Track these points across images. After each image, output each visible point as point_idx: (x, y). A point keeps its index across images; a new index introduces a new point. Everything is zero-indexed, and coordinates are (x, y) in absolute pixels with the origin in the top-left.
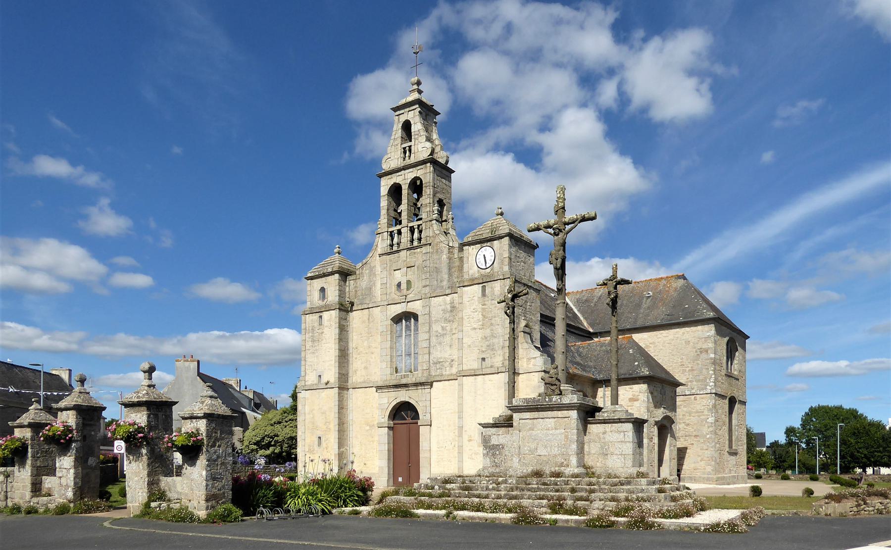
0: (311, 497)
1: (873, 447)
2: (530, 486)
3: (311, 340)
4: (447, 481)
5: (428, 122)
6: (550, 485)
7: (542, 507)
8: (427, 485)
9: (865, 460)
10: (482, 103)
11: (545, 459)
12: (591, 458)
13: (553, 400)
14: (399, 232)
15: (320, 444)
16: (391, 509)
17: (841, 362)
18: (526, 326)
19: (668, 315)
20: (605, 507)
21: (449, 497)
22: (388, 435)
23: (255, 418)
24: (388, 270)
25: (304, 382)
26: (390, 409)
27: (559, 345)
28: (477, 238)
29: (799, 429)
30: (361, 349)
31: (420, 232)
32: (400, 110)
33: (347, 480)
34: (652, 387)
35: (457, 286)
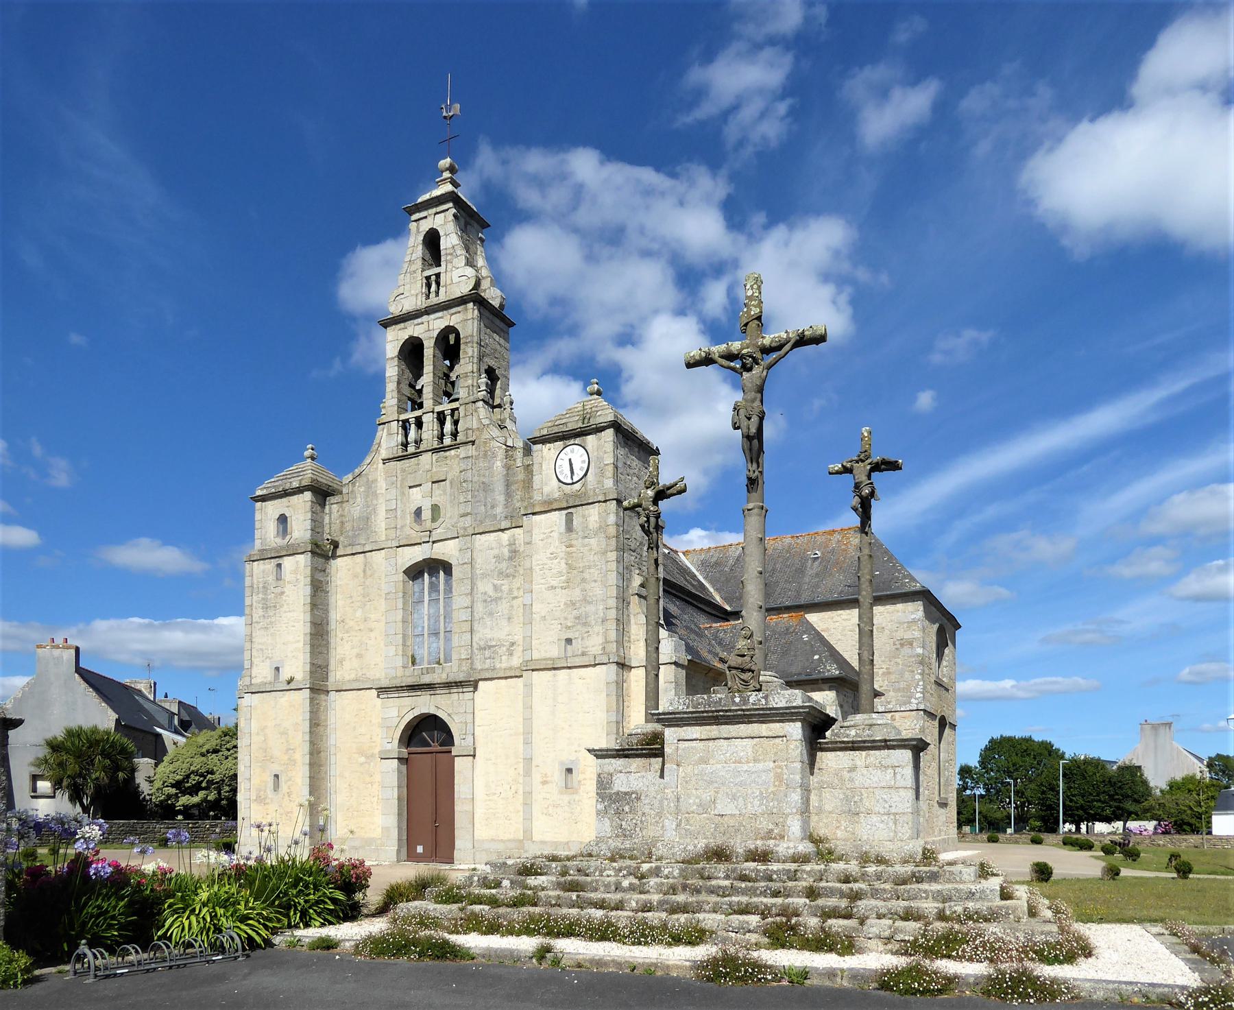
0: (222, 911)
1: (1091, 794)
2: (714, 882)
3: (261, 605)
4: (528, 870)
5: (469, 237)
6: (755, 880)
7: (749, 931)
8: (485, 878)
9: (1081, 812)
10: (537, 298)
11: (732, 822)
13: (751, 701)
14: (419, 423)
15: (276, 787)
16: (407, 940)
17: (1007, 681)
18: (642, 585)
19: (849, 586)
21: (535, 905)
22: (399, 771)
23: (175, 743)
24: (399, 486)
25: (248, 679)
26: (402, 727)
27: (753, 593)
28: (556, 430)
29: (976, 768)
30: (351, 623)
31: (456, 423)
32: (419, 212)
33: (311, 868)
34: (842, 697)
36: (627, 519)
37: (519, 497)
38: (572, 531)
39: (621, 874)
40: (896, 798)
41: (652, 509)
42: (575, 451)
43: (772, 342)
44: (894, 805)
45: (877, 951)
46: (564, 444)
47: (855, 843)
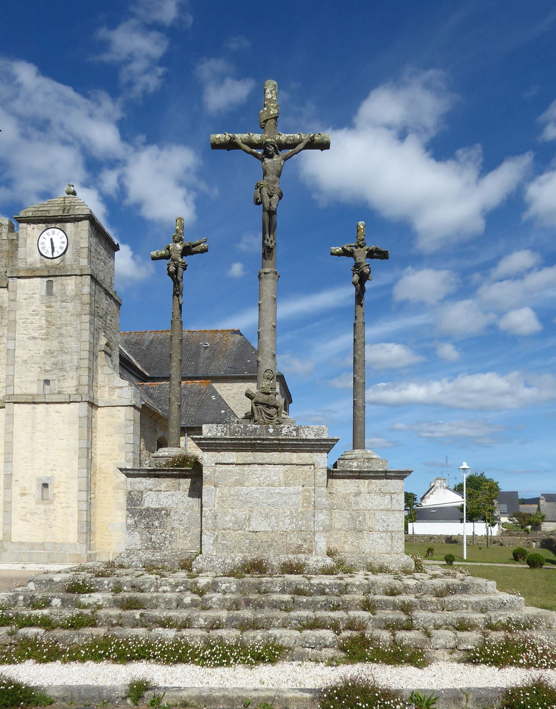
7: (326, 646)
11: (265, 538)
12: (335, 536)
13: (284, 432)
18: (107, 345)
20: (459, 643)
21: (94, 625)
27: (268, 343)
28: (39, 214)
35: (8, 274)
36: (97, 292)
37: (4, 264)
38: (51, 295)
39: (178, 590)
40: (392, 519)
41: (180, 260)
42: (56, 233)
43: (287, 139)
44: (391, 524)
45: (444, 660)
46: (47, 226)
47: (360, 555)
